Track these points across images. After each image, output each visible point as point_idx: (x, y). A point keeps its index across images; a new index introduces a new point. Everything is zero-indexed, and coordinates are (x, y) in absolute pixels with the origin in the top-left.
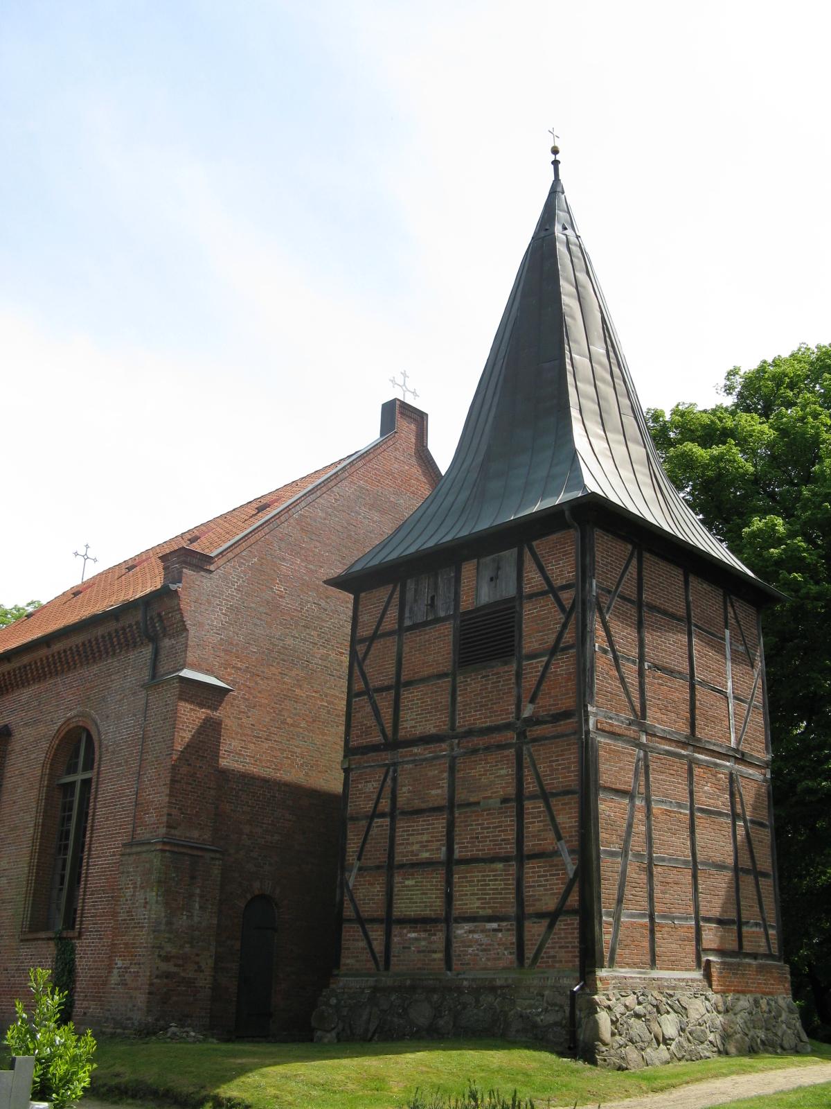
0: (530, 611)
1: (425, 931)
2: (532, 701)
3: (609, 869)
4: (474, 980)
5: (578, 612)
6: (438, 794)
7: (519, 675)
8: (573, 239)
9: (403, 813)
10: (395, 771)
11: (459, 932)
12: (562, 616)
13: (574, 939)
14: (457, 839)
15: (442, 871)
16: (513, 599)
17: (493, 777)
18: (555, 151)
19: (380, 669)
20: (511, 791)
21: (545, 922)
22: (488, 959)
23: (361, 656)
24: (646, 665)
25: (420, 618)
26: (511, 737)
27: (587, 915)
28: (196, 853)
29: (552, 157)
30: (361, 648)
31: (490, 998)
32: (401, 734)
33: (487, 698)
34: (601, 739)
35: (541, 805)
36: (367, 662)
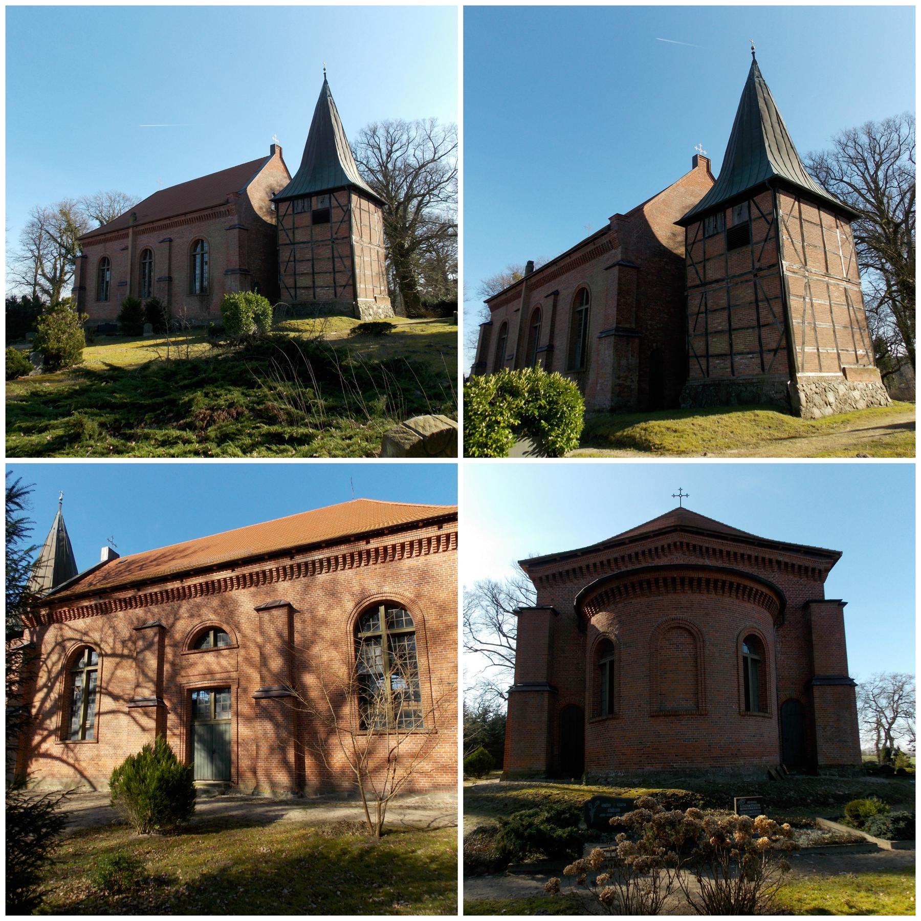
13: (785, 360)
26: (751, 276)
33: (321, 232)
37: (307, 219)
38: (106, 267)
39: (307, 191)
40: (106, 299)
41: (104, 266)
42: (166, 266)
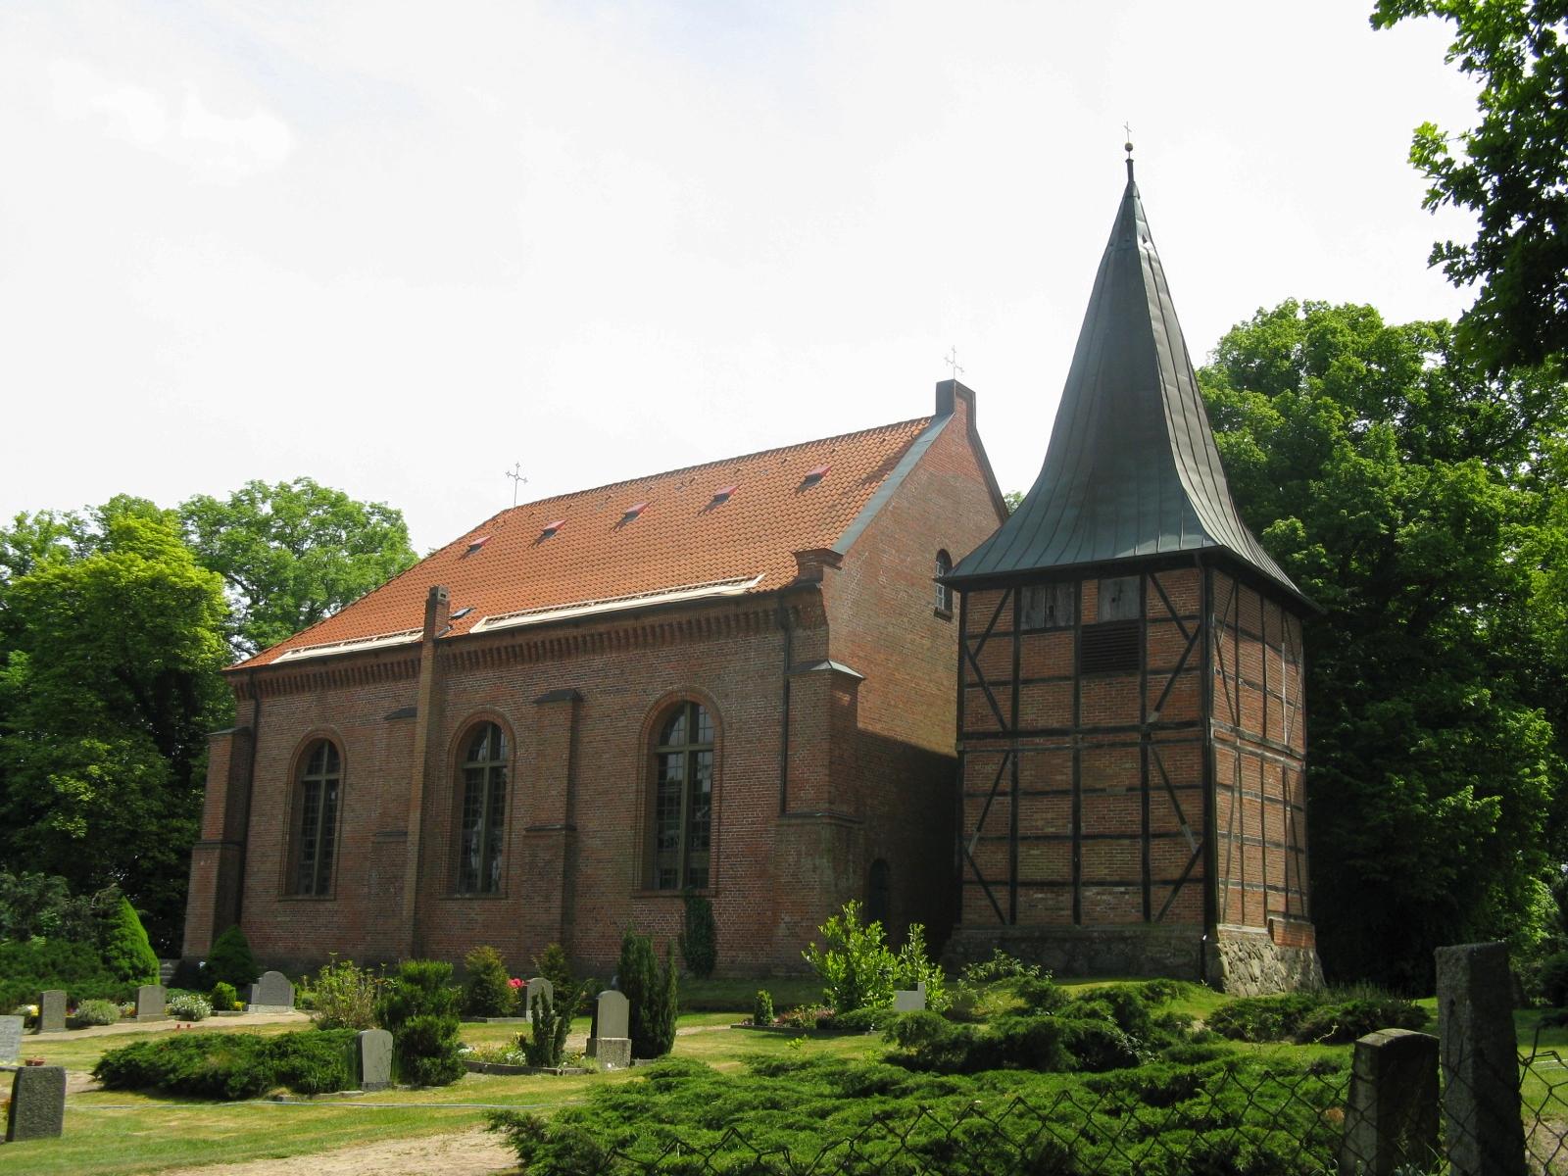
0: (1152, 633)
1: (1052, 892)
2: (1158, 709)
3: (1222, 846)
4: (1104, 932)
5: (1201, 640)
6: (1063, 778)
7: (1143, 686)
8: (1152, 252)
9: (1026, 793)
10: (1015, 757)
11: (1087, 894)
12: (1185, 641)
13: (1199, 901)
14: (1083, 818)
15: (1070, 844)
16: (1137, 621)
17: (1119, 769)
18: (1129, 148)
19: (996, 662)
20: (1137, 781)
21: (1171, 888)
22: (1115, 916)
23: (972, 651)
24: (1240, 680)
25: (1039, 623)
26: (1137, 737)
27: (1209, 883)
28: (848, 825)
29: (1125, 155)
30: (972, 645)
31: (1122, 946)
32: (1022, 725)
33: (1108, 702)
34: (1218, 746)
35: (1166, 795)
36: (980, 657)
37: (1059, 653)
38: (323, 777)
39: (1048, 561)
40: (323, 889)
41: (314, 769)
42: (557, 789)
